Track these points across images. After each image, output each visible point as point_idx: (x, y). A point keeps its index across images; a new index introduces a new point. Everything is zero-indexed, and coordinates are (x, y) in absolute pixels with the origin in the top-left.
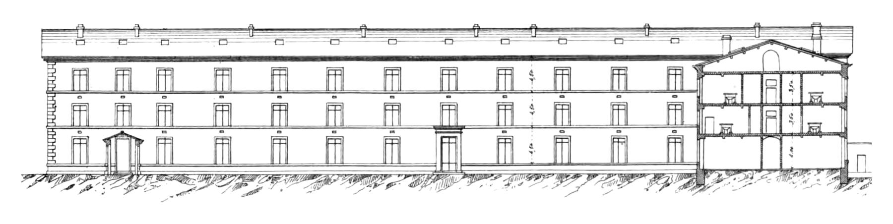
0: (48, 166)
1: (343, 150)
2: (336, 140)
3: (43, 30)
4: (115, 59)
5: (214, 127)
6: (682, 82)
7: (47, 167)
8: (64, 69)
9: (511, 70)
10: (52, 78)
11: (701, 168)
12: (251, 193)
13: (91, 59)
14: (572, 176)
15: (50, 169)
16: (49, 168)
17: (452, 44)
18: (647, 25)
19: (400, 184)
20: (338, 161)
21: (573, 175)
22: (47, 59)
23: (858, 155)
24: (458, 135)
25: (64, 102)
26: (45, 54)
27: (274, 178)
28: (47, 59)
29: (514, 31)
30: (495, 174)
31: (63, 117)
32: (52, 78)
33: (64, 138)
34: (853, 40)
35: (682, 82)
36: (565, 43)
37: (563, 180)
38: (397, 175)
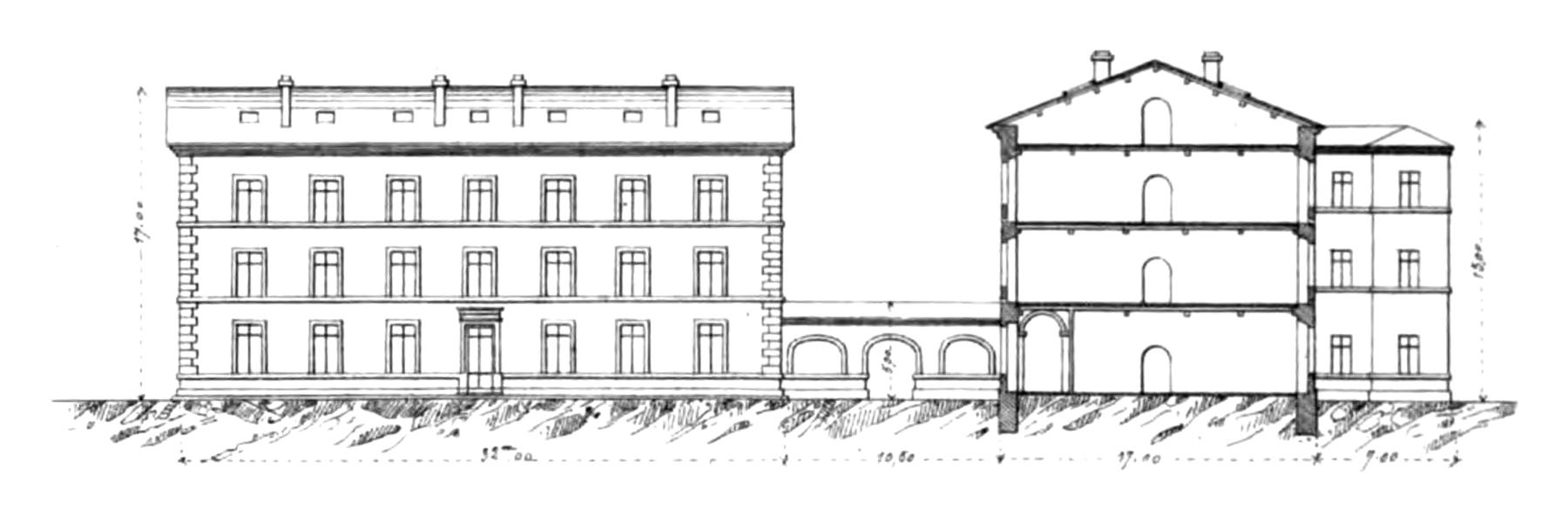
0: (180, 380)
1: (418, 349)
2: (714, 328)
3: (168, 89)
4: (386, 150)
5: (388, 299)
6: (574, 207)
7: (177, 382)
8: (216, 174)
9: (570, 181)
10: (190, 196)
11: (1012, 387)
12: (305, 429)
13: (582, 150)
14: (441, 405)
15: (185, 384)
16: (183, 382)
17: (641, 120)
18: (519, 78)
19: (70, 410)
20: (639, 368)
21: (445, 402)
22: (178, 149)
23: (792, 90)
24: (497, 324)
25: (216, 249)
26: (172, 140)
27: (625, 405)
28: (178, 149)
29: (255, 93)
30: (839, 399)
31: (214, 278)
32: (190, 196)
33: (215, 324)
34: (793, 108)
35: (574, 207)
36: (256, 120)
37: (1424, 411)
38: (1489, 402)
